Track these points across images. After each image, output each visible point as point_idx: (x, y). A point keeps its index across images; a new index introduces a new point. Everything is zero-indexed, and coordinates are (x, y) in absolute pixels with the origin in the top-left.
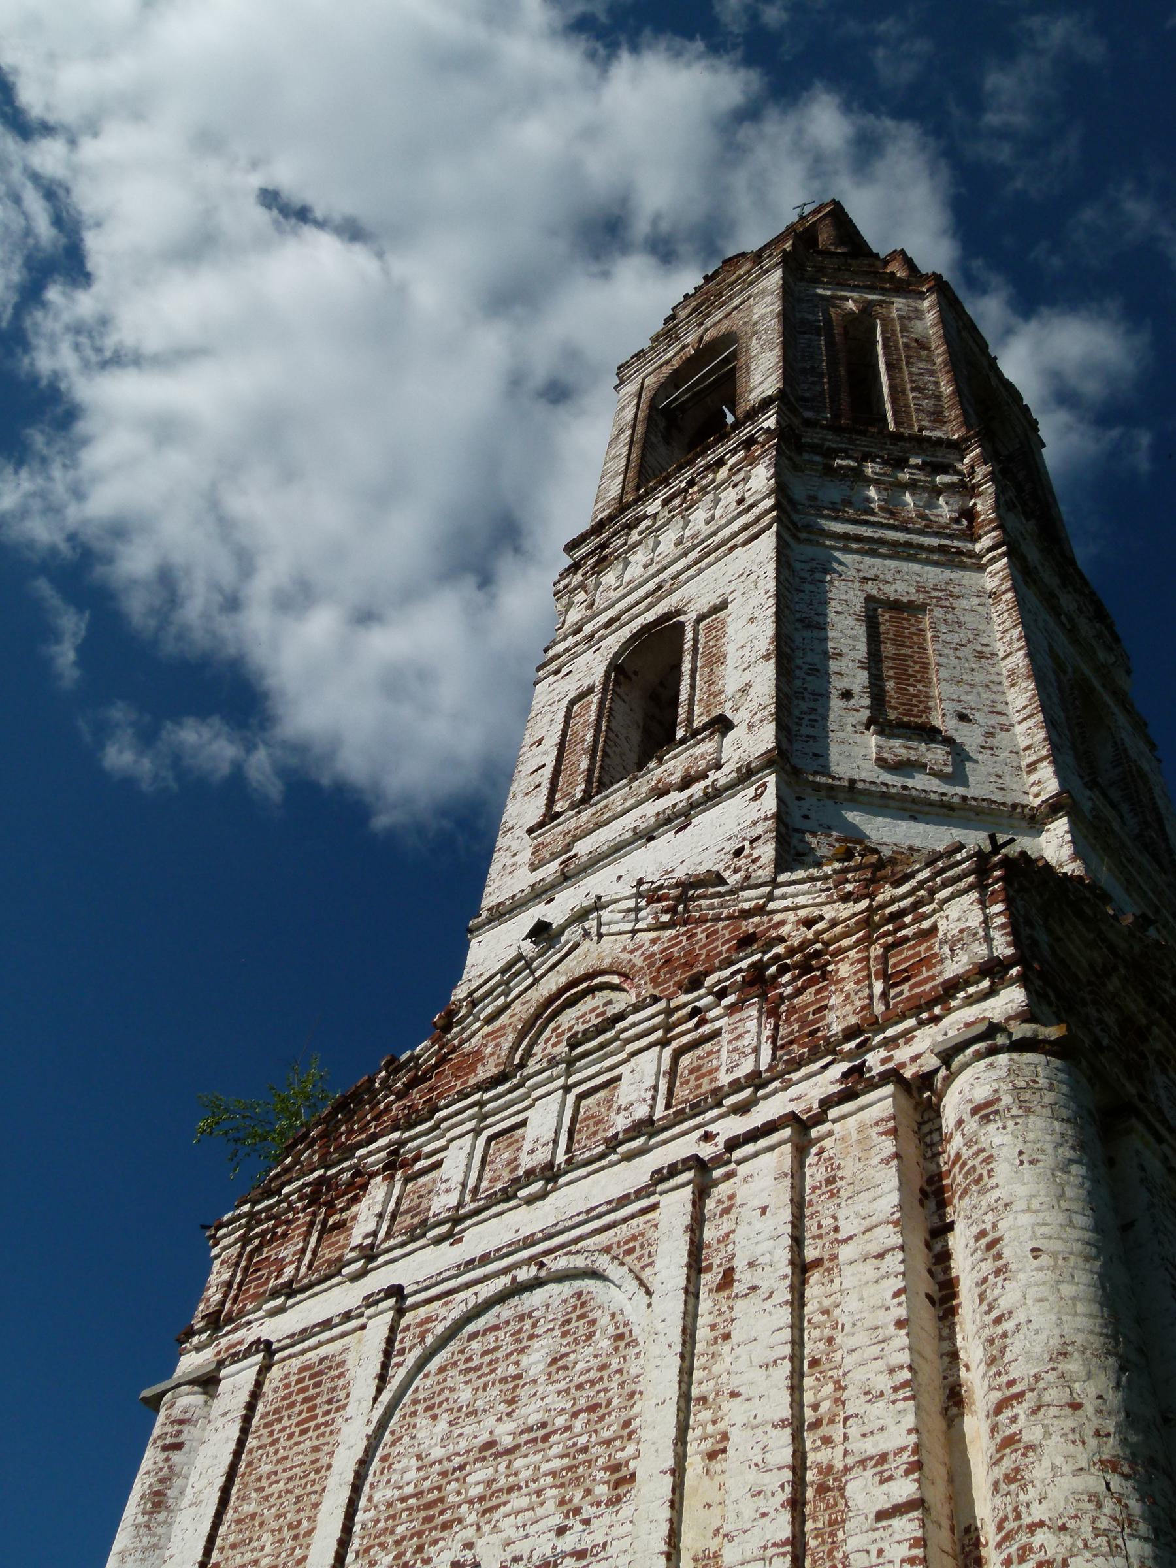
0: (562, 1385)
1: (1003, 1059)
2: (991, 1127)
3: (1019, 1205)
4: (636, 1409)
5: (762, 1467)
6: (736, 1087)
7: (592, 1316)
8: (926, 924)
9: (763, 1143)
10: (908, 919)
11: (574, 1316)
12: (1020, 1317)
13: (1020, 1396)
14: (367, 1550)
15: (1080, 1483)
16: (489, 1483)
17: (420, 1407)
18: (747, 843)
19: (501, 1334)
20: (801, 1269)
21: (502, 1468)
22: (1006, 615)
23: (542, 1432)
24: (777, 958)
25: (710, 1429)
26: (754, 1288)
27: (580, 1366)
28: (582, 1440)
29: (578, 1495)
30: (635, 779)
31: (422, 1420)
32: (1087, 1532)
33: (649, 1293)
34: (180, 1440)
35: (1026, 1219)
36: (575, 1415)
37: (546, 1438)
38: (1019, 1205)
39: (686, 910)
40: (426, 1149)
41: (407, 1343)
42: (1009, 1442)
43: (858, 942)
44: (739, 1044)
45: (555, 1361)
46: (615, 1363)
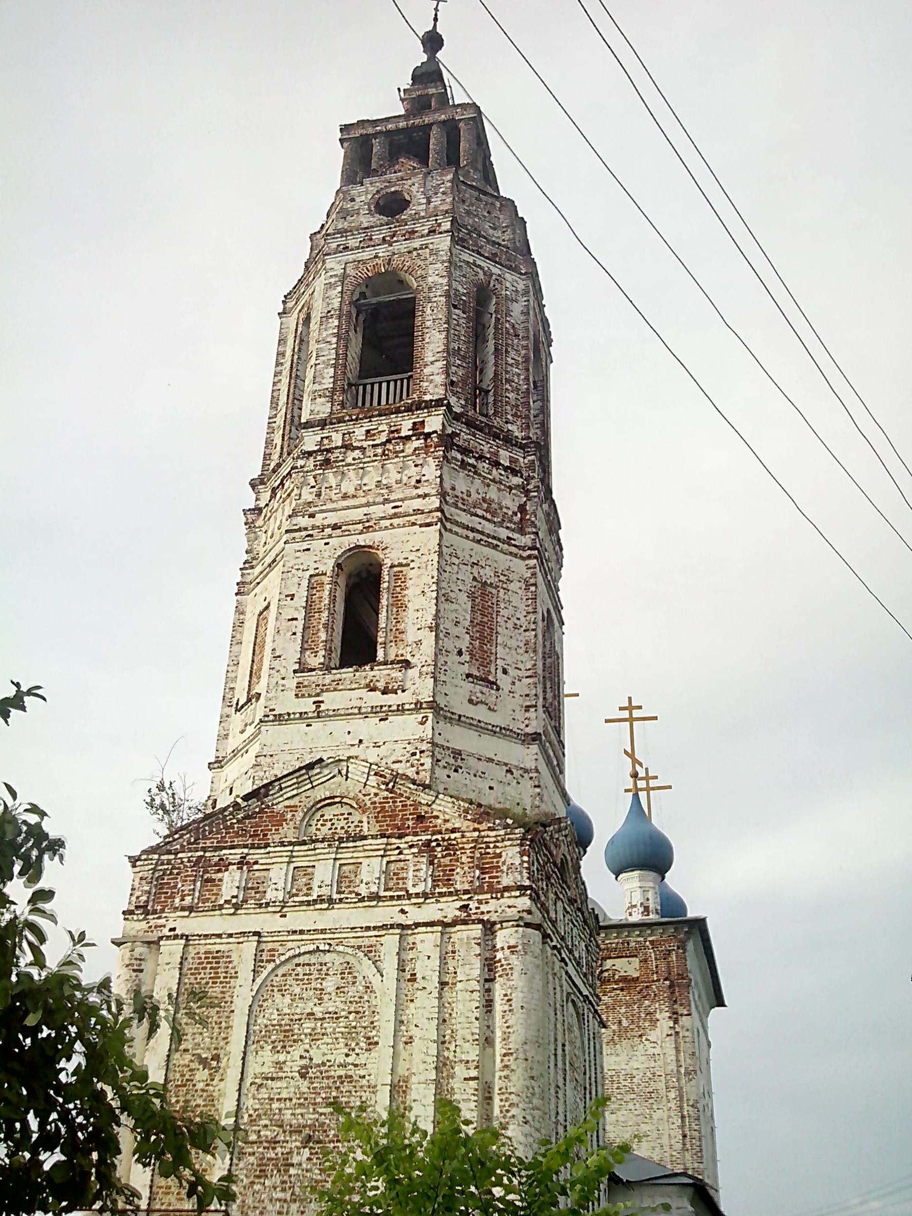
0: (343, 999)
1: (521, 929)
2: (514, 956)
3: (519, 989)
4: (376, 1019)
5: (427, 1054)
6: (417, 895)
7: (355, 974)
8: (498, 851)
9: (429, 929)
10: (492, 845)
11: (346, 971)
12: (515, 1028)
13: (512, 1054)
14: (258, 1042)
15: (524, 1083)
16: (313, 1029)
17: (276, 989)
18: (418, 752)
19: (312, 968)
20: (443, 984)
21: (319, 1024)
22: (530, 601)
23: (335, 1016)
24: (437, 840)
25: (405, 1033)
26: (425, 988)
27: (350, 994)
28: (354, 1024)
29: (353, 1045)
30: (357, 671)
31: (277, 995)
32: (524, 1097)
33: (382, 976)
34: (142, 968)
35: (521, 995)
36: (350, 1013)
37: (337, 1018)
38: (519, 989)
39: (393, 787)
40: (261, 861)
41: (341, 1024)
42: (506, 1066)
43: (471, 848)
44: (418, 873)
45: (338, 988)
46: (366, 998)
